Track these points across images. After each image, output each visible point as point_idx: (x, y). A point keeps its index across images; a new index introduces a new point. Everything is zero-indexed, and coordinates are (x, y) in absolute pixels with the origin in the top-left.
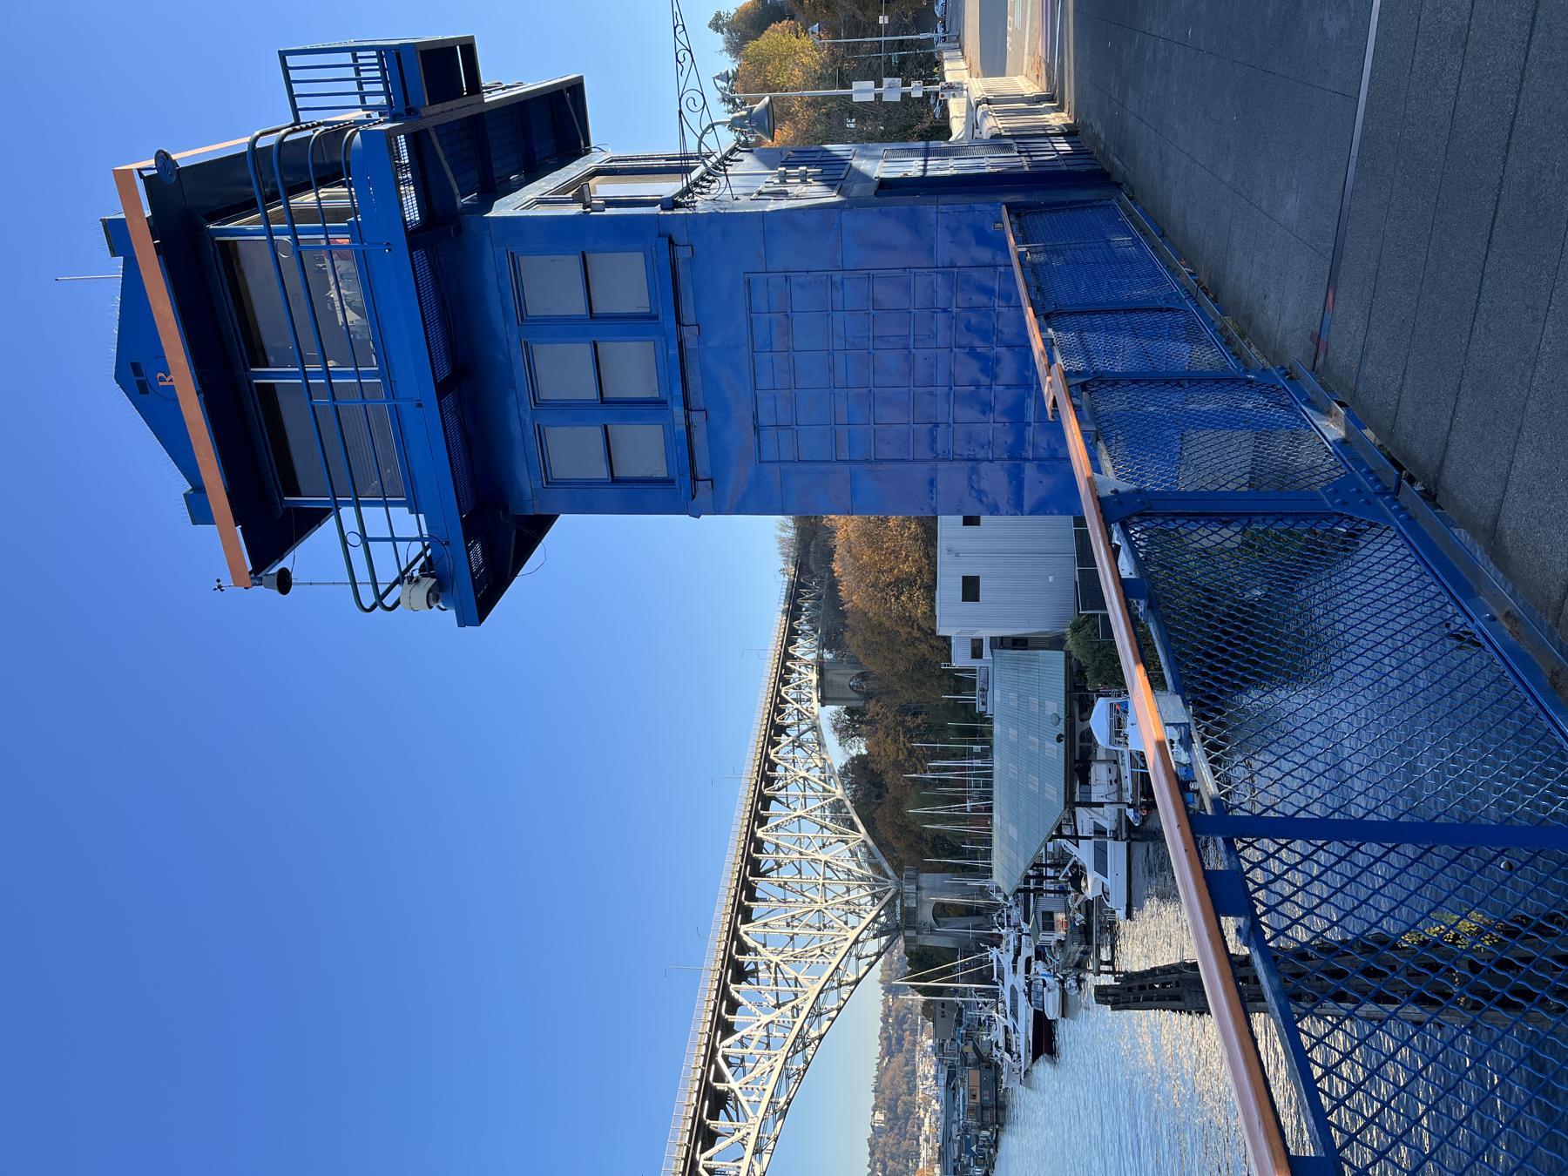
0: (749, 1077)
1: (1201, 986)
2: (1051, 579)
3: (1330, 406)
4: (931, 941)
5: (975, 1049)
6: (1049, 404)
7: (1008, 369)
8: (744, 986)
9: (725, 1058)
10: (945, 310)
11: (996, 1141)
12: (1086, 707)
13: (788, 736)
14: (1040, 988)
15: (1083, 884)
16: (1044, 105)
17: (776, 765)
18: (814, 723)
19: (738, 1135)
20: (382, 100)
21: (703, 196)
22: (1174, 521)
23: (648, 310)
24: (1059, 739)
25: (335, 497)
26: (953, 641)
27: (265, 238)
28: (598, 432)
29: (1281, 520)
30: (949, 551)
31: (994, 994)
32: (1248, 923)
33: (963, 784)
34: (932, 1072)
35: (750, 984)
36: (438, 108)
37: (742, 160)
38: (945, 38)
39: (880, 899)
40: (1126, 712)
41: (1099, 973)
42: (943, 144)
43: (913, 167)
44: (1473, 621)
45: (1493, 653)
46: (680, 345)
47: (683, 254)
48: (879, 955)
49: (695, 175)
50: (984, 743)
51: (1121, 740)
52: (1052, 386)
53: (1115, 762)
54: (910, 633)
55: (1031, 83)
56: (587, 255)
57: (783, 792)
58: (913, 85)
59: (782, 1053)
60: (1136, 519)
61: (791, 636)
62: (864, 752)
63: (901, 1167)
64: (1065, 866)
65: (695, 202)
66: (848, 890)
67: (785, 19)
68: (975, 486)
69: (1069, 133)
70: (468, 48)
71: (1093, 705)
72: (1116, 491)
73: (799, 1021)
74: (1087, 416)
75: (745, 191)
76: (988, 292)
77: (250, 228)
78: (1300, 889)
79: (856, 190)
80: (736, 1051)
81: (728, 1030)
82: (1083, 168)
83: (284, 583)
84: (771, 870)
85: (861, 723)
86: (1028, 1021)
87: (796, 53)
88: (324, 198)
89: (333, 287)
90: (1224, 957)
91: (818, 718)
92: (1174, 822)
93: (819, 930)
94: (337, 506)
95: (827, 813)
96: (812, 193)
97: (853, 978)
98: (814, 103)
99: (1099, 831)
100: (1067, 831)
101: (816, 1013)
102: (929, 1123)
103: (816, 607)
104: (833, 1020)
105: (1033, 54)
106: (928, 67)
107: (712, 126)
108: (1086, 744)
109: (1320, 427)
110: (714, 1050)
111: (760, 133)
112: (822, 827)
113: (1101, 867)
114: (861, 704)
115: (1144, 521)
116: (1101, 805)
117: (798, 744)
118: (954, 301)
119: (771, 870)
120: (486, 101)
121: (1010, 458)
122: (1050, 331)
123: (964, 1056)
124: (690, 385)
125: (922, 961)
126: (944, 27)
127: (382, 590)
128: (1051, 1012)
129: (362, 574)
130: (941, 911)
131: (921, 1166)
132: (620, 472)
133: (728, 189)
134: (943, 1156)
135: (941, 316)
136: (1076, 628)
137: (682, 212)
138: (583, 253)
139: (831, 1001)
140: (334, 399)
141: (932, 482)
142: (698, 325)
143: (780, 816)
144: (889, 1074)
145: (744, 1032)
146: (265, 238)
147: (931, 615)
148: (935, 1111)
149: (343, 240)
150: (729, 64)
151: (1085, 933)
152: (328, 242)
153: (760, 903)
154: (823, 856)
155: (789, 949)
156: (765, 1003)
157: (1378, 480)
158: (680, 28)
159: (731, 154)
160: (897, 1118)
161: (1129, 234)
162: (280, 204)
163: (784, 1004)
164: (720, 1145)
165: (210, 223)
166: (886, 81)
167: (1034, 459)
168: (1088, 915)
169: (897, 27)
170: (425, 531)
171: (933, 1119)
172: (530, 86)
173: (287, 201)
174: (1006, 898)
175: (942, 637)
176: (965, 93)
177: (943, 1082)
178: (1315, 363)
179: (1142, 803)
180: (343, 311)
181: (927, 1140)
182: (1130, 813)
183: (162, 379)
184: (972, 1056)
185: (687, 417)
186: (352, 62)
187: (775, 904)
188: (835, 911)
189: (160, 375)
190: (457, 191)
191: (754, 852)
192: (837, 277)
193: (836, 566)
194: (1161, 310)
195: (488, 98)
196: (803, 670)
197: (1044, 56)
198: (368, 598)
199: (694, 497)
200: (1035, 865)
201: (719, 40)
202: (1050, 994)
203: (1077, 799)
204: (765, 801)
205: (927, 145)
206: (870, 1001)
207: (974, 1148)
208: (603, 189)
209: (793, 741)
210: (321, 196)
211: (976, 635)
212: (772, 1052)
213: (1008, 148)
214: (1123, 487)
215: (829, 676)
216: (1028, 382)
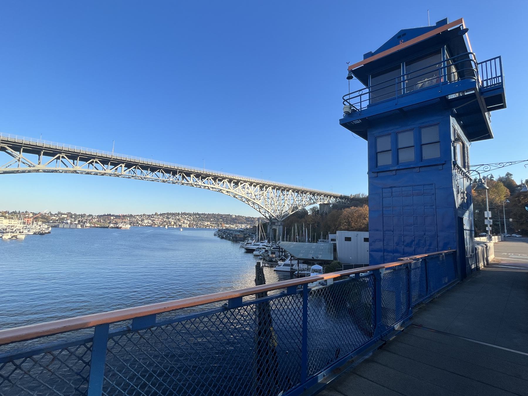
0: (241, 189)
2: (351, 258)
3: (403, 327)
4: (268, 228)
5: (247, 237)
6: (402, 259)
7: (407, 249)
8: (259, 188)
9: (245, 185)
10: (425, 234)
11: (230, 240)
12: (320, 264)
13: (312, 197)
14: (259, 250)
15: (281, 261)
16: (485, 262)
17: (306, 194)
18: (315, 202)
19: (230, 188)
20: (485, 85)
21: (457, 172)
22: (373, 286)
23: (423, 159)
24: (313, 258)
25: (371, 87)
26: (335, 235)
27: (442, 60)
28: (389, 148)
29: (374, 312)
30: (357, 234)
31: (258, 241)
32: (285, 294)
33: (302, 236)
34: (243, 228)
35: (260, 189)
36: (483, 100)
37: (468, 182)
39: (277, 217)
40: (319, 273)
41: (263, 263)
42: (473, 235)
43: (466, 226)
44: (351, 353)
45: (343, 356)
46: (414, 168)
47: (440, 167)
48: (266, 217)
49: (463, 169)
50: (311, 240)
51: (313, 271)
52: (407, 259)
53: (308, 270)
54: (337, 225)
55: (492, 259)
56: (391, 151)
57: (300, 196)
58: (490, 228)
59: (246, 197)
60: (374, 277)
61: (335, 197)
62: (309, 214)
63: (225, 221)
64: (285, 257)
65: (455, 170)
66: (279, 210)
67: (510, 193)
68: (377, 241)
69: (477, 268)
70: (503, 107)
71: (321, 266)
72: (381, 273)
73: (252, 200)
74: (400, 267)
75: (459, 183)
76: (430, 245)
77: (445, 56)
79: (460, 212)
80: (246, 187)
81: (251, 185)
82: (467, 271)
83: (350, 78)
84: (283, 194)
85: (315, 214)
86: (253, 248)
87: (499, 196)
88: (454, 74)
89: (428, 79)
90: (267, 290)
91: (317, 203)
93: (271, 204)
94: (369, 88)
95: (295, 206)
96: (458, 201)
97: (261, 211)
98: (484, 201)
99: (292, 265)
100: (292, 258)
101: (254, 203)
102: (233, 226)
103: (343, 202)
104: (252, 207)
105: (502, 260)
106: (495, 232)
107: (479, 174)
108: (312, 264)
109: (397, 324)
110: (246, 182)
111: (477, 187)
112: (292, 204)
113: (285, 265)
114: (320, 213)
115: (373, 279)
116: (298, 266)
117: (311, 199)
118: (427, 236)
119: (283, 194)
120: (485, 113)
121: (384, 249)
122: (421, 260)
123: (246, 234)
124: (402, 171)
125: (265, 225)
126: (509, 236)
127: (348, 101)
128: (255, 253)
129: (351, 96)
130: (275, 230)
131: (225, 225)
132: (379, 155)
133: (459, 178)
134: (227, 229)
135: (423, 233)
136: (339, 263)
137: (452, 166)
138: (440, 142)
139: (256, 207)
140: (397, 83)
141: (377, 230)
142: (419, 172)
144: (242, 219)
145: (250, 188)
146: (442, 60)
147: (341, 230)
148: (235, 228)
149: (442, 80)
150: (495, 179)
151: (271, 261)
152: (442, 77)
153: (276, 191)
154: (286, 205)
155: (267, 198)
156: (255, 193)
157: (384, 336)
158: (510, 164)
159: (469, 179)
160: (234, 220)
161: (448, 282)
162: (452, 63)
163: (255, 197)
164: (229, 184)
165: (446, 46)
166: (491, 221)
167: (384, 255)
168: (275, 262)
169: (508, 224)
170: (363, 109)
171: (234, 228)
172: (490, 124)
173: (453, 65)
174: (278, 244)
175: (336, 232)
176: (489, 241)
177: (241, 229)
178: (414, 325)
179: (299, 275)
180: (422, 83)
181: (230, 226)
182: (297, 272)
183: (401, 41)
184: (246, 236)
185: (394, 170)
186: (493, 77)
187: (276, 194)
188: (274, 207)
189: (403, 40)
190: (457, 108)
192: (434, 207)
193: (353, 208)
194: (427, 288)
195: (486, 114)
196: (328, 200)
197: (501, 263)
198: (346, 98)
199: (373, 172)
200: (285, 251)
201: (503, 175)
202: (258, 253)
203: (299, 261)
204: (298, 192)
205: (473, 231)
206: (256, 215)
207: (228, 236)
208: (458, 146)
209: (311, 198)
210: (455, 73)
211: (337, 240)
212: (246, 194)
213: (473, 252)
214: (382, 275)
215: (326, 206)
216: (405, 254)
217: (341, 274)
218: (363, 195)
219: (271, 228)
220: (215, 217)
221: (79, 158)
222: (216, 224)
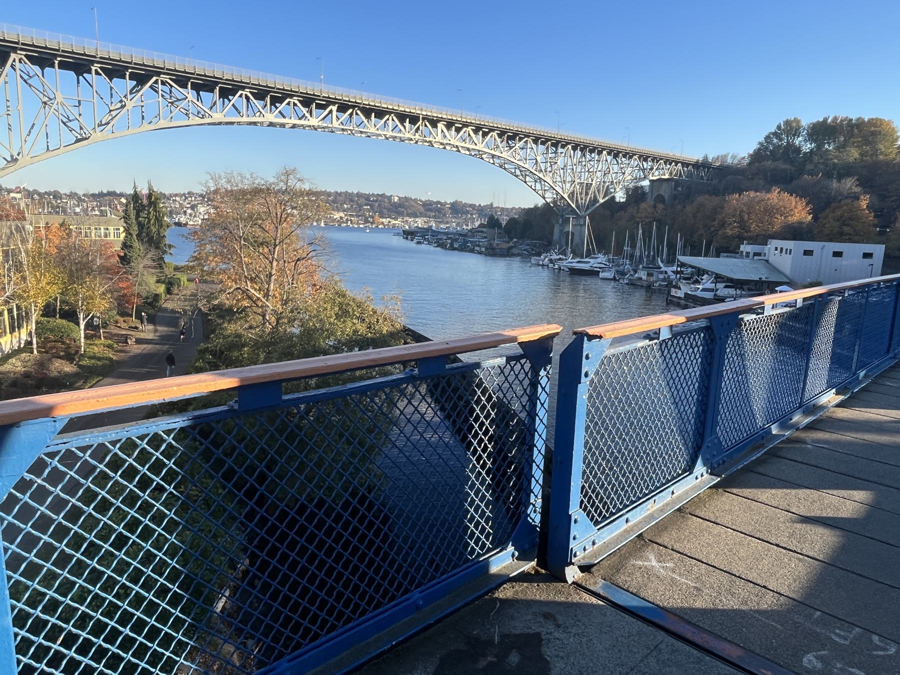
1: (303, 357)
24: (760, 278)
38: (71, 315)
63: (376, 209)
78: (506, 379)
92: (329, 363)
99: (717, 290)
110: (529, 137)
143: (537, 150)
144: (415, 205)
160: (396, 208)
191: (220, 87)
217: (195, 418)
218: (734, 157)
219: (561, 231)
220: (352, 200)
221: (218, 88)
222: (358, 216)
